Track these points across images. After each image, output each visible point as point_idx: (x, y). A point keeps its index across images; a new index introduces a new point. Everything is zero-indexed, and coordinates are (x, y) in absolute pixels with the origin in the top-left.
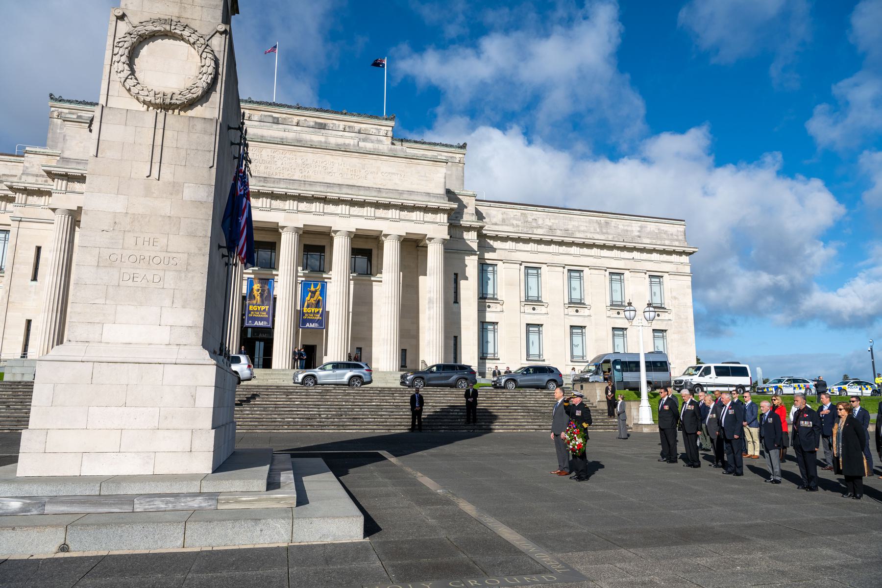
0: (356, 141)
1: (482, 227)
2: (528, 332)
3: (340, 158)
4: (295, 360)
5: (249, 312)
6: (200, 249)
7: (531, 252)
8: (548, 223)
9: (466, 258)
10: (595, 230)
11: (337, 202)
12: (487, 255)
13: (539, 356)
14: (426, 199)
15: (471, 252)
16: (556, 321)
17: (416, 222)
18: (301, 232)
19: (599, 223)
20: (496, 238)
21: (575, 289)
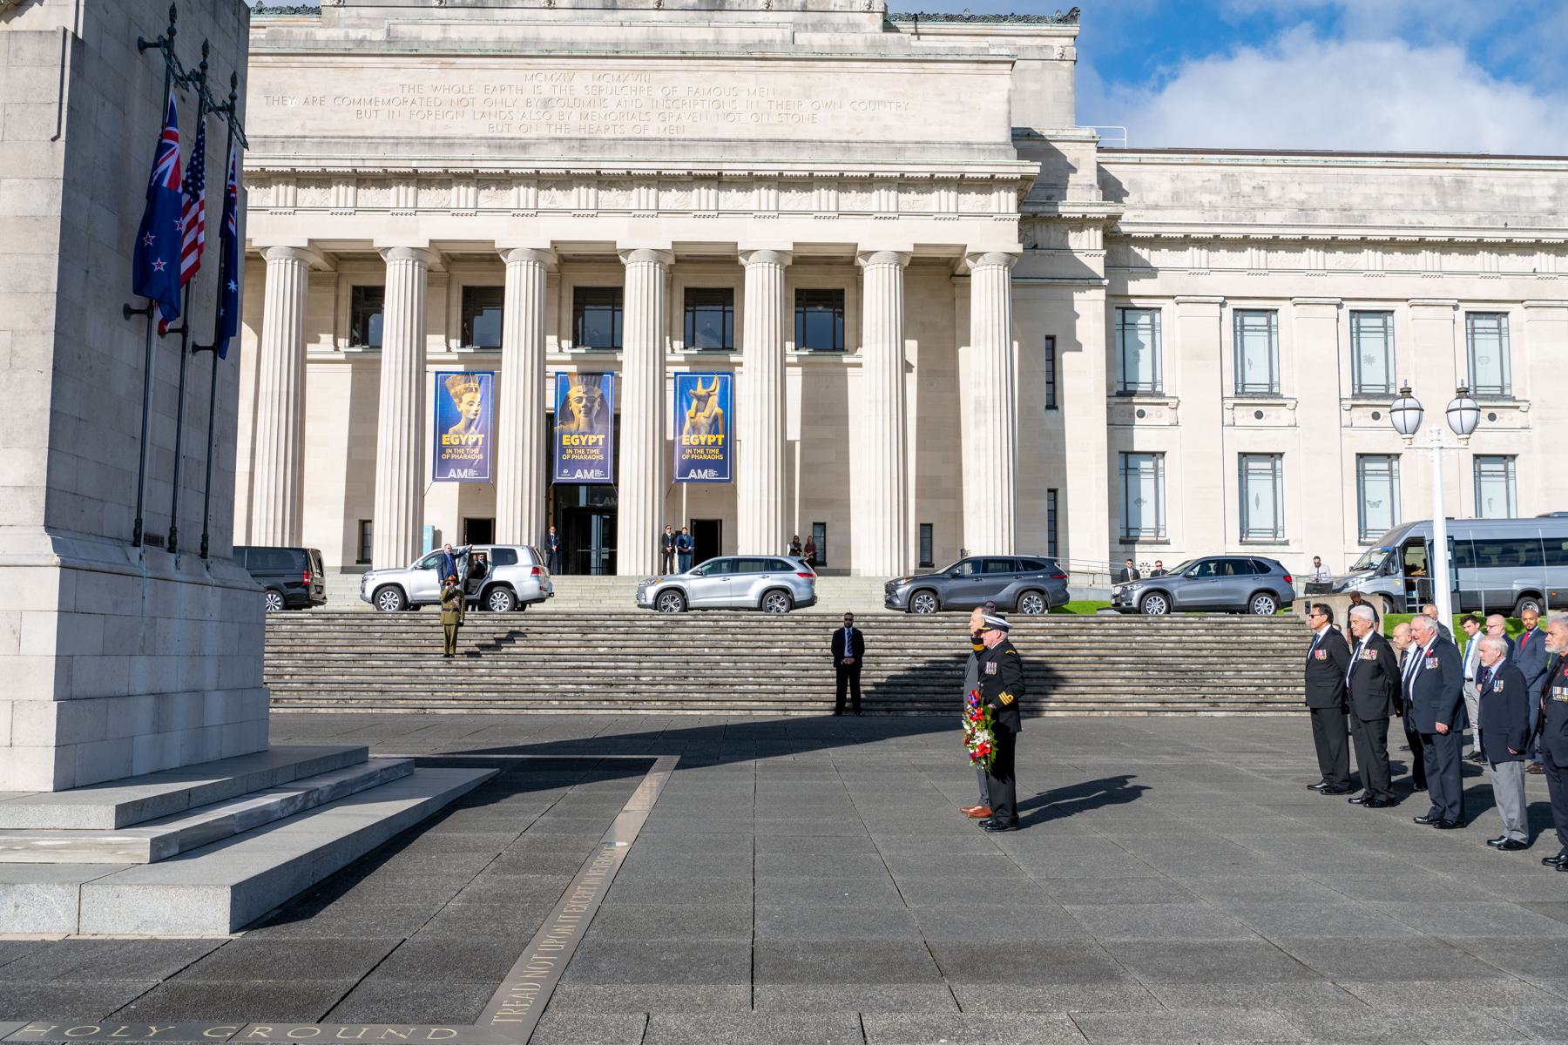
0: (788, 32)
1: (1115, 218)
2: (1243, 475)
3: (752, 77)
4: (667, 556)
5: (563, 450)
6: (36, 321)
7: (1251, 271)
8: (1297, 193)
9: (1077, 296)
10: (1426, 203)
11: (749, 182)
12: (1134, 287)
13: (1275, 532)
14: (962, 157)
15: (1090, 281)
16: (1317, 442)
17: (938, 216)
18: (789, 262)
19: (1437, 185)
20: (1156, 242)
21: (1370, 360)
